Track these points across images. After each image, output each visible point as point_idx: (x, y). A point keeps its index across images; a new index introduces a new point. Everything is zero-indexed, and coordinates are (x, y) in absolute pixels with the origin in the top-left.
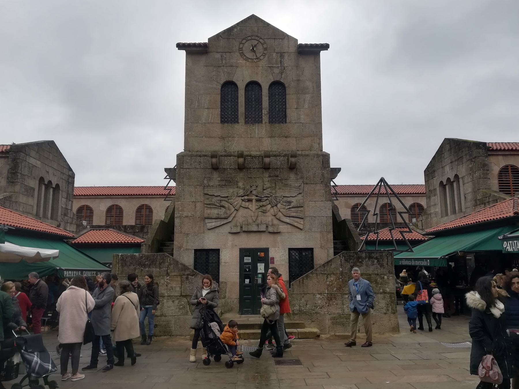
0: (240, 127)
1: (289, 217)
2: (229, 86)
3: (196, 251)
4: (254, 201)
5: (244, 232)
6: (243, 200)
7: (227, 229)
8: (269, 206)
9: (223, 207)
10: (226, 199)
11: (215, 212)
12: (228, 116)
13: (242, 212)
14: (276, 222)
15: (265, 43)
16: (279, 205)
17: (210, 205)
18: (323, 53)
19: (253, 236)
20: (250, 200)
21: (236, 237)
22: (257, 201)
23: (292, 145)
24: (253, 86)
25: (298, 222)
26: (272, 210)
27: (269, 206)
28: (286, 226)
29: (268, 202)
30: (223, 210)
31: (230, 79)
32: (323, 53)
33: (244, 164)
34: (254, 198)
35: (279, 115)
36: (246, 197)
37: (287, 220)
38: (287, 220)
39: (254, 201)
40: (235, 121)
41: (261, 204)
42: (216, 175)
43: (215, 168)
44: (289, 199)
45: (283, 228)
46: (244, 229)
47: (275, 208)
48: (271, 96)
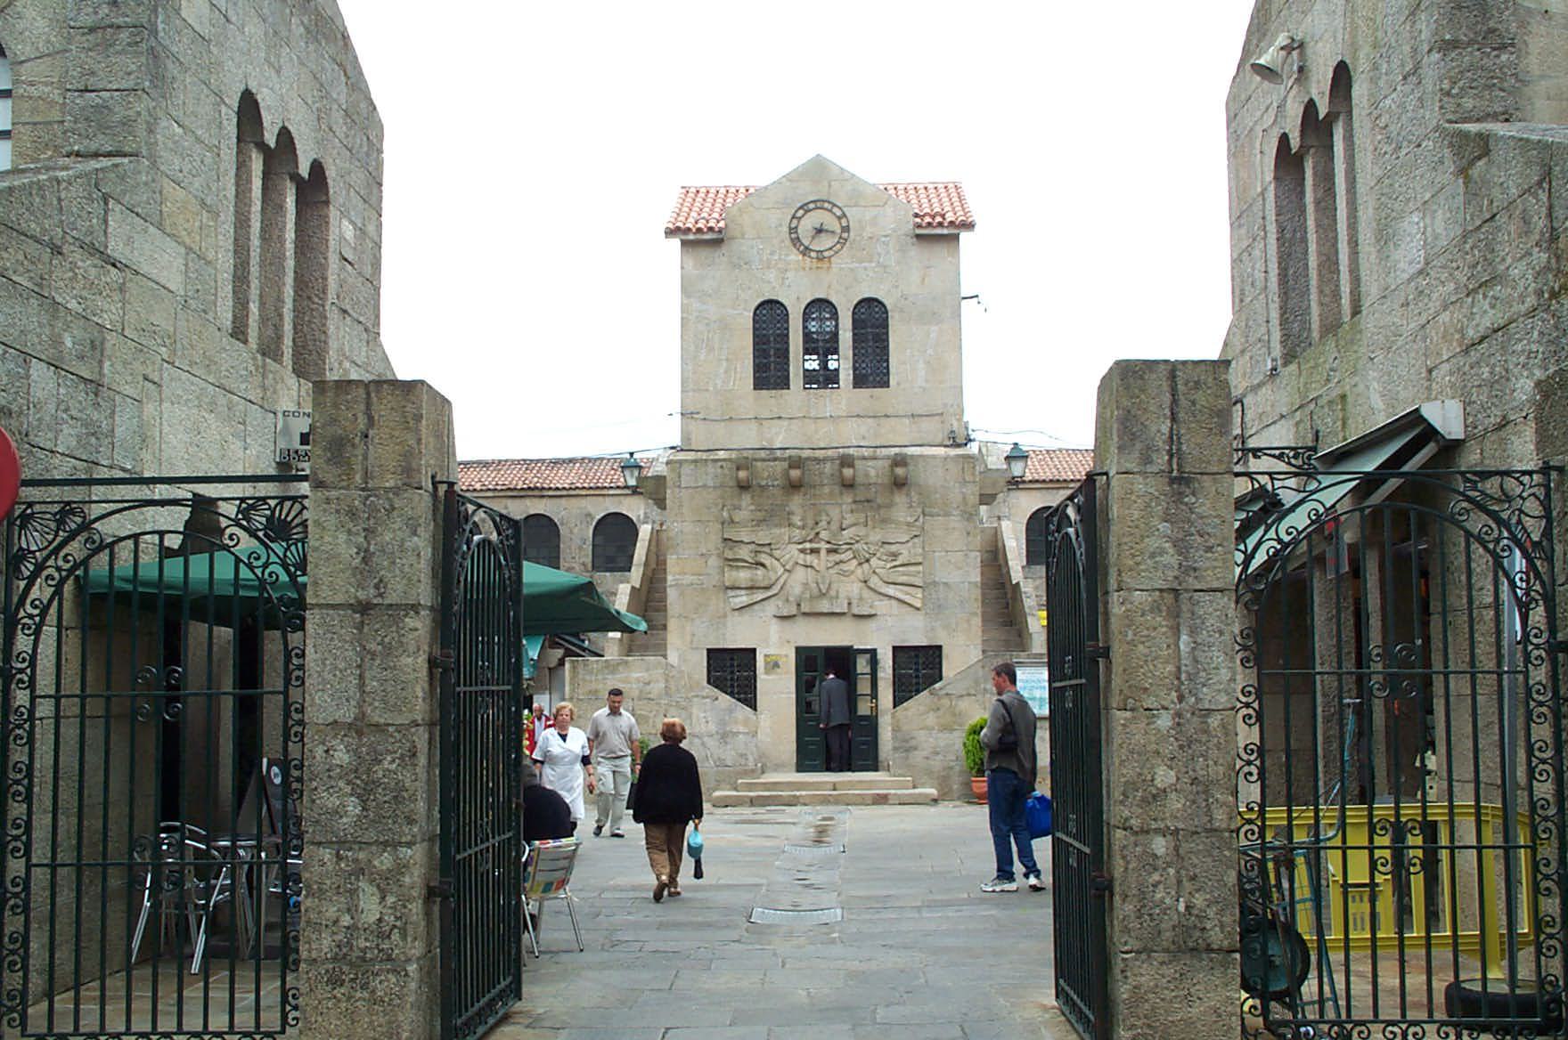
0: (796, 395)
1: (132, 791)
2: (770, 315)
3: (709, 651)
4: (823, 553)
5: (805, 614)
6: (802, 551)
7: (770, 608)
8: (855, 562)
9: (763, 565)
10: (766, 549)
11: (743, 576)
12: (770, 370)
13: (800, 574)
14: (867, 594)
15: (844, 215)
16: (874, 561)
17: (732, 563)
18: (964, 236)
19: (827, 624)
20: (814, 551)
21: (786, 624)
22: (829, 551)
23: (899, 435)
24: (820, 307)
26: (859, 571)
27: (855, 562)
28: (886, 602)
29: (849, 554)
30: (760, 572)
31: (713, 790)
32: (964, 236)
33: (800, 480)
34: (824, 546)
35: (872, 372)
36: (808, 545)
37: (891, 590)
38: (891, 590)
39: (823, 553)
40: (784, 383)
41: (837, 557)
42: (746, 499)
43: (744, 487)
44: (893, 548)
45: (881, 606)
46: (805, 608)
47: (866, 566)
48: (856, 324)
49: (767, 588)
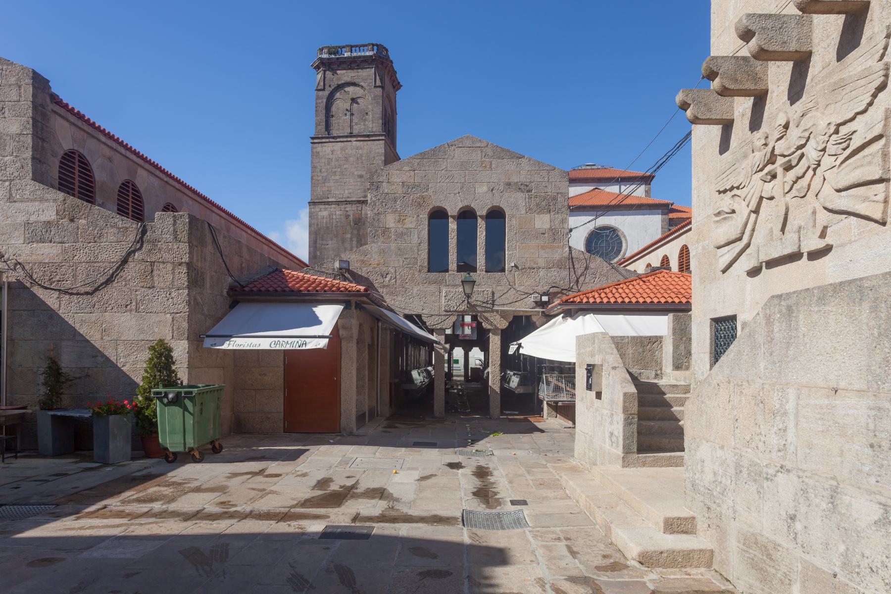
25: (866, 199)
49: (740, 239)
